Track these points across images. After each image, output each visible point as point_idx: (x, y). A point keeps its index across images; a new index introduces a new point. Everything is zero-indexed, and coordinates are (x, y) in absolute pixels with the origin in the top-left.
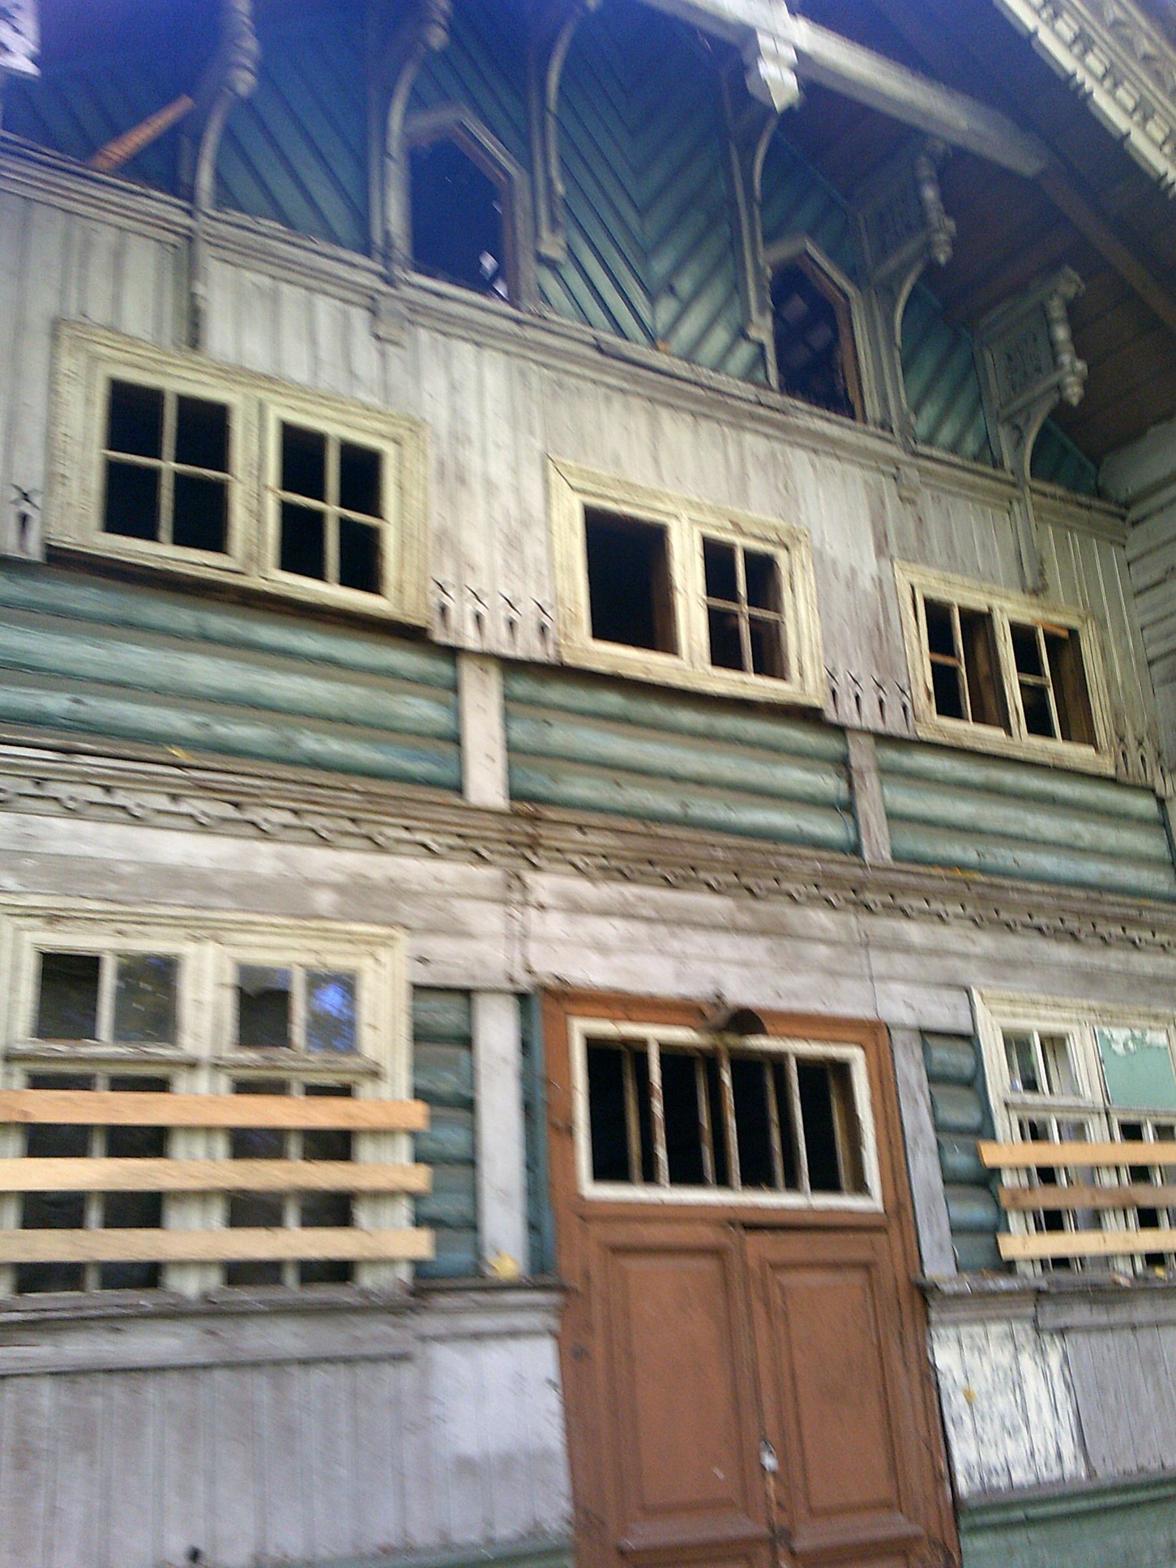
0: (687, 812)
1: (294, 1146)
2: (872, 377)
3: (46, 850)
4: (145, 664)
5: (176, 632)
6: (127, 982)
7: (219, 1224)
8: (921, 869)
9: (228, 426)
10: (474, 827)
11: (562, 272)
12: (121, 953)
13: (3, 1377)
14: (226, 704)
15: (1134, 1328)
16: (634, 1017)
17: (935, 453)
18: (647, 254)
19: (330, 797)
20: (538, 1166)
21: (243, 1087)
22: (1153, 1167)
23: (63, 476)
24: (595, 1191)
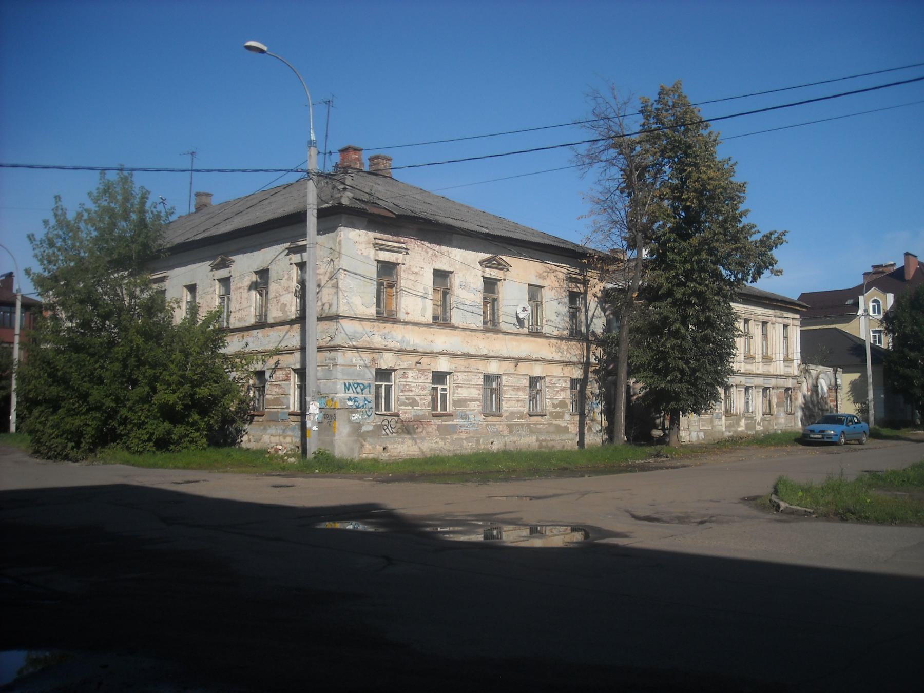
2: (395, 238)
3: (906, 531)
4: (603, 404)
6: (74, 441)
7: (438, 247)
11: (194, 159)
14: (472, 237)
17: (781, 382)
18: (705, 434)
19: (397, 248)
20: (522, 519)
23: (56, 215)
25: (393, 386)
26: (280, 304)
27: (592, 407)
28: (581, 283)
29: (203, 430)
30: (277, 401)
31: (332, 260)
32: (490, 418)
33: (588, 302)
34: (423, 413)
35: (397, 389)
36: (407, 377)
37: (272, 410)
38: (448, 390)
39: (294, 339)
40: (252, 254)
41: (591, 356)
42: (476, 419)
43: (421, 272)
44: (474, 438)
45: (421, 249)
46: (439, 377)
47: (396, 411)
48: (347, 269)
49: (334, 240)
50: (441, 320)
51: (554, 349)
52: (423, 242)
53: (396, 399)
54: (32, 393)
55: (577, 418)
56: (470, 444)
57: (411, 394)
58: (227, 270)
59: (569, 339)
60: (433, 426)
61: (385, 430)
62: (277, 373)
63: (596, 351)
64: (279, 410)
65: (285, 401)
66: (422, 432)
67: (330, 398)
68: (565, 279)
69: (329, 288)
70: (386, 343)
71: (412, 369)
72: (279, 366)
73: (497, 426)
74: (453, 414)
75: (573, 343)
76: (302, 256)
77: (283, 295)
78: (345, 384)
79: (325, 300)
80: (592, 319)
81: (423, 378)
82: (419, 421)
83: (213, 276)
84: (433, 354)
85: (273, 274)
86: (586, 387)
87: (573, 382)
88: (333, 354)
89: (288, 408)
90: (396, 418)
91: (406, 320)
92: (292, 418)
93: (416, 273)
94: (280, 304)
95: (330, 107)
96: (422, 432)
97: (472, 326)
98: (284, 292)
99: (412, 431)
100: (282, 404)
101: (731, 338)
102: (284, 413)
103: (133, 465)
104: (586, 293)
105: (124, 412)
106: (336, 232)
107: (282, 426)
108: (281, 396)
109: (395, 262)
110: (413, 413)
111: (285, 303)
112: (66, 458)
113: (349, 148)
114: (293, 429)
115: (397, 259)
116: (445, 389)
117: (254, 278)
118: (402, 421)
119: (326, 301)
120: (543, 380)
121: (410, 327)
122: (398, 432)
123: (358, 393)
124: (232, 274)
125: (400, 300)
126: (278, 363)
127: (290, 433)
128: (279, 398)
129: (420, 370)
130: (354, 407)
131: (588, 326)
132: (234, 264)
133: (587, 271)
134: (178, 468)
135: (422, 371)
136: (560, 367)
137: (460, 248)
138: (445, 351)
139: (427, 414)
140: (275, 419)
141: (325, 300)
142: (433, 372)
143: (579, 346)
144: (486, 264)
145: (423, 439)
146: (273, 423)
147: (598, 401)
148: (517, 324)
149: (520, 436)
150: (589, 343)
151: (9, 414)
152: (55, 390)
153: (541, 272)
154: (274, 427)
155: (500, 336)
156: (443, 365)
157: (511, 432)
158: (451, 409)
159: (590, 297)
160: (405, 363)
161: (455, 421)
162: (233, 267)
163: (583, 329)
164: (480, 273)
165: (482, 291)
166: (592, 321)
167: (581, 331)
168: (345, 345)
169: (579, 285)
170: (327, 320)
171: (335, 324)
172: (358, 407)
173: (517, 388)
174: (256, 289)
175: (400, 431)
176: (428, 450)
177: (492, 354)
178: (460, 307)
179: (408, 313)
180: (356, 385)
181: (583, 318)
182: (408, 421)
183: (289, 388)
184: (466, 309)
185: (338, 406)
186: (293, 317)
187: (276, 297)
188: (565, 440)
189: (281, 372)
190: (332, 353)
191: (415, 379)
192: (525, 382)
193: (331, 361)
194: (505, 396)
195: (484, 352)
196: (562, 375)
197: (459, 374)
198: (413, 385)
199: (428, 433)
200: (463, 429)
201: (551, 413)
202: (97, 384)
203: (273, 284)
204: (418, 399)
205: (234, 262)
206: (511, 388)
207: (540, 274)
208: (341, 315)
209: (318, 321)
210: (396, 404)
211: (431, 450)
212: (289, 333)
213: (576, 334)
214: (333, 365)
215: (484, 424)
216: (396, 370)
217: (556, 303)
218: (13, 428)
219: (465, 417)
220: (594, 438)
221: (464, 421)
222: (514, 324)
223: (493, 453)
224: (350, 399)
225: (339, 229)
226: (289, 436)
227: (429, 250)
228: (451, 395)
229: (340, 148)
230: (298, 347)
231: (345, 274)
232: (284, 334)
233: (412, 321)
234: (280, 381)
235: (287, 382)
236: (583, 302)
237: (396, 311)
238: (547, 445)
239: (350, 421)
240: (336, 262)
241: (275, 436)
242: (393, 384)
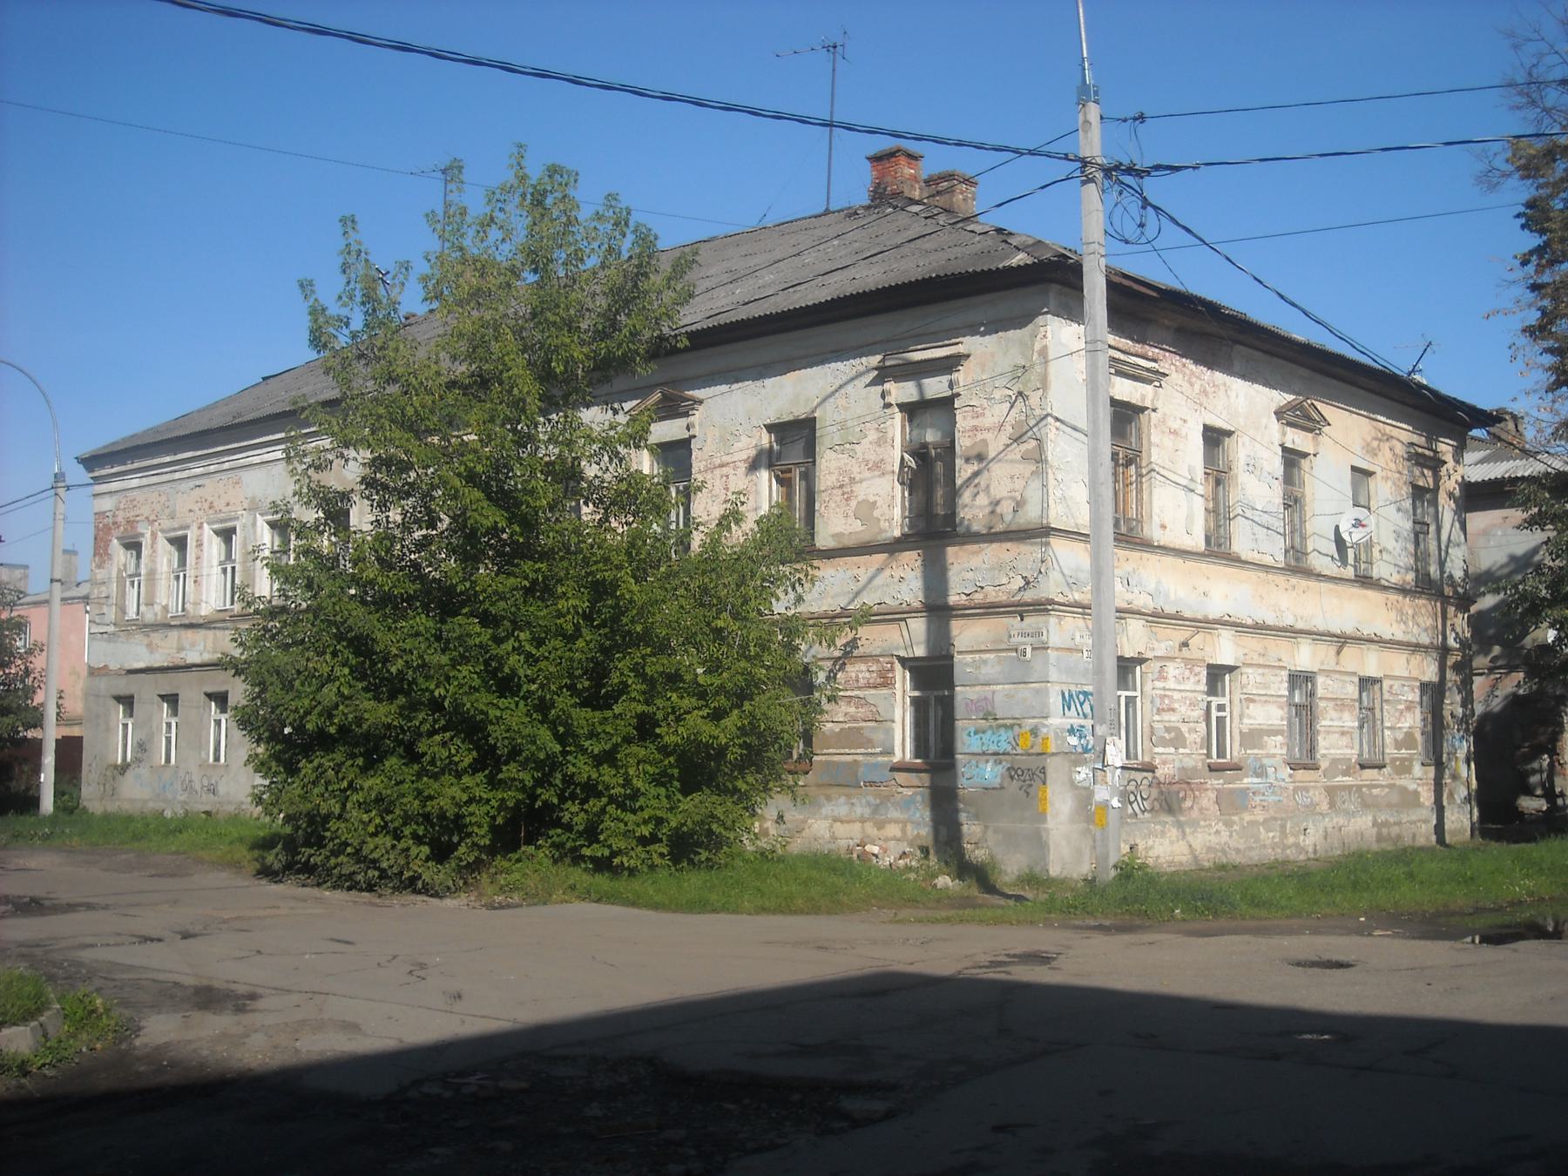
2: (1138, 348)
19: (1148, 370)
25: (1138, 700)
26: (853, 503)
27: (1453, 746)
28: (1428, 468)
30: (852, 737)
31: (1020, 394)
32: (1300, 774)
33: (1440, 509)
34: (1193, 763)
35: (1148, 705)
36: (1166, 679)
37: (836, 758)
38: (1228, 709)
39: (904, 586)
40: (759, 383)
41: (1448, 632)
42: (1280, 776)
43: (1183, 432)
44: (1275, 819)
45: (1181, 376)
46: (1217, 675)
47: (1147, 759)
48: (1061, 417)
49: (1027, 347)
50: (1217, 550)
51: (1393, 615)
52: (1184, 360)
53: (1147, 730)
54: (313, 717)
55: (1431, 771)
56: (1271, 835)
57: (1173, 719)
58: (681, 423)
59: (1416, 592)
60: (1209, 793)
61: (1131, 803)
62: (849, 668)
63: (1455, 620)
64: (860, 758)
65: (878, 736)
66: (1192, 807)
67: (1028, 728)
68: (1406, 456)
69: (1012, 461)
70: (1129, 596)
71: (1172, 659)
72: (856, 653)
73: (1311, 793)
74: (1242, 764)
75: (1421, 602)
76: (920, 387)
77: (861, 481)
78: (1063, 694)
79: (999, 491)
80: (1447, 547)
81: (1192, 679)
82: (1185, 781)
84: (1207, 624)
85: (827, 435)
86: (1443, 702)
87: (1424, 687)
88: (1031, 621)
89: (889, 752)
90: (1149, 775)
91: (1162, 544)
92: (901, 777)
93: (1175, 433)
94: (853, 503)
95: (839, 58)
96: (1192, 807)
97: (1268, 560)
98: (867, 474)
99: (1175, 806)
100: (869, 743)
102: (876, 766)
103: (633, 904)
104: (1437, 488)
105: (581, 768)
106: (1030, 326)
107: (870, 798)
108: (864, 724)
109: (1140, 404)
110: (1177, 764)
111: (872, 499)
112: (412, 885)
113: (899, 151)
114: (907, 804)
115: (1143, 397)
116: (1221, 708)
117: (765, 439)
118: (1160, 783)
119: (1005, 494)
120: (1377, 687)
121: (1169, 560)
122: (1152, 809)
123: (1085, 716)
124: (696, 431)
125: (1151, 494)
126: (853, 643)
127: (894, 814)
128: (862, 728)
129: (1186, 660)
130: (1080, 750)
131: (1442, 564)
132: (701, 408)
133: (1437, 440)
135: (1190, 663)
136: (1405, 656)
137: (1244, 377)
138: (1227, 618)
139: (1200, 764)
140: (847, 781)
141: (999, 491)
142: (1208, 665)
143: (1430, 608)
144: (1289, 416)
145: (1194, 824)
146: (841, 790)
147: (1461, 733)
148: (1336, 556)
149: (1346, 812)
150: (1445, 601)
152: (378, 713)
153: (1369, 439)
154: (843, 799)
155: (1313, 584)
156: (1225, 649)
157: (1332, 805)
158: (1235, 754)
159: (1443, 498)
160: (1163, 645)
161: (1245, 780)
162: (697, 417)
163: (1433, 570)
164: (1277, 438)
165: (1281, 478)
166: (1447, 552)
167: (1429, 575)
168: (1060, 599)
169: (1426, 471)
170: (1010, 540)
171: (1037, 548)
172: (1086, 750)
173: (1340, 704)
174: (770, 466)
175: (1157, 806)
176: (1204, 851)
177: (1300, 625)
178: (1249, 513)
179: (1163, 527)
180: (1081, 697)
181: (1433, 546)
182: (1170, 783)
183: (893, 706)
184: (1256, 519)
185: (1052, 748)
186: (897, 533)
187: (841, 487)
188: (1414, 822)
189: (863, 667)
190: (1028, 620)
191: (1179, 683)
192: (1352, 690)
193: (1028, 640)
194: (1324, 723)
195: (1288, 620)
196: (1406, 674)
198: (1176, 696)
199: (1201, 809)
200: (1257, 798)
201: (1394, 760)
203: (829, 454)
204: (1184, 728)
205: (701, 402)
206: (1331, 704)
207: (1368, 444)
208: (1052, 526)
210: (1147, 742)
211: (1209, 849)
212: (888, 572)
213: (1426, 586)
214: (1033, 649)
215: (1291, 787)
216: (1146, 660)
217: (1393, 508)
218: (47, 803)
219: (1260, 772)
220: (1460, 819)
221: (1259, 780)
222: (1332, 557)
224: (1071, 731)
225: (1040, 320)
226: (896, 822)
227: (1194, 380)
228: (1236, 720)
229: (871, 153)
230: (917, 604)
231: (1057, 429)
232: (870, 574)
233: (1172, 545)
234: (859, 688)
235: (885, 691)
236: (1432, 510)
237: (1139, 521)
238: (1389, 834)
239: (1072, 784)
240: (1034, 399)
241: (848, 822)
242: (1138, 693)
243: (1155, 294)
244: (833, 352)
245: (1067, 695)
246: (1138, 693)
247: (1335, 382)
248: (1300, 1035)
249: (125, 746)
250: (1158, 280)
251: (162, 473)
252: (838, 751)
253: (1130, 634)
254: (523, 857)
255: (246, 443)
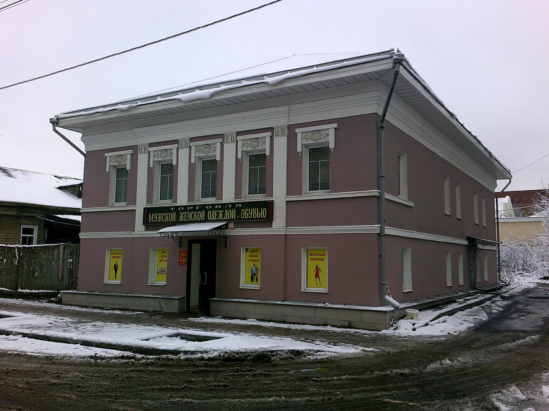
0: (81, 198)
1: (489, 291)
5: (279, 82)
8: (35, 332)
9: (262, 352)
10: (346, 227)
12: (168, 335)
13: (1, 88)
15: (104, 304)
16: (22, 204)
21: (257, 281)
22: (80, 243)
24: (206, 283)
29: (503, 194)
83: (414, 325)
101: (501, 266)
134: (176, 232)
151: (187, 304)
197: (537, 393)
202: (510, 405)
209: (248, 251)
223: (53, 337)
243: (457, 300)
244: (437, 296)
245: (78, 328)
246: (22, 235)
247: (218, 83)
248: (60, 291)
249: (119, 233)
250: (256, 74)
251: (252, 287)
252: (118, 249)
253: (352, 321)
254: (145, 382)
255: (146, 296)
